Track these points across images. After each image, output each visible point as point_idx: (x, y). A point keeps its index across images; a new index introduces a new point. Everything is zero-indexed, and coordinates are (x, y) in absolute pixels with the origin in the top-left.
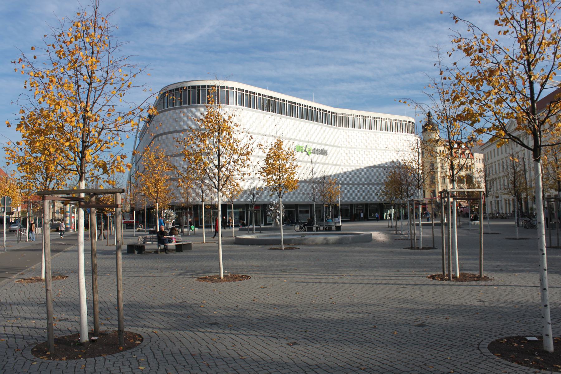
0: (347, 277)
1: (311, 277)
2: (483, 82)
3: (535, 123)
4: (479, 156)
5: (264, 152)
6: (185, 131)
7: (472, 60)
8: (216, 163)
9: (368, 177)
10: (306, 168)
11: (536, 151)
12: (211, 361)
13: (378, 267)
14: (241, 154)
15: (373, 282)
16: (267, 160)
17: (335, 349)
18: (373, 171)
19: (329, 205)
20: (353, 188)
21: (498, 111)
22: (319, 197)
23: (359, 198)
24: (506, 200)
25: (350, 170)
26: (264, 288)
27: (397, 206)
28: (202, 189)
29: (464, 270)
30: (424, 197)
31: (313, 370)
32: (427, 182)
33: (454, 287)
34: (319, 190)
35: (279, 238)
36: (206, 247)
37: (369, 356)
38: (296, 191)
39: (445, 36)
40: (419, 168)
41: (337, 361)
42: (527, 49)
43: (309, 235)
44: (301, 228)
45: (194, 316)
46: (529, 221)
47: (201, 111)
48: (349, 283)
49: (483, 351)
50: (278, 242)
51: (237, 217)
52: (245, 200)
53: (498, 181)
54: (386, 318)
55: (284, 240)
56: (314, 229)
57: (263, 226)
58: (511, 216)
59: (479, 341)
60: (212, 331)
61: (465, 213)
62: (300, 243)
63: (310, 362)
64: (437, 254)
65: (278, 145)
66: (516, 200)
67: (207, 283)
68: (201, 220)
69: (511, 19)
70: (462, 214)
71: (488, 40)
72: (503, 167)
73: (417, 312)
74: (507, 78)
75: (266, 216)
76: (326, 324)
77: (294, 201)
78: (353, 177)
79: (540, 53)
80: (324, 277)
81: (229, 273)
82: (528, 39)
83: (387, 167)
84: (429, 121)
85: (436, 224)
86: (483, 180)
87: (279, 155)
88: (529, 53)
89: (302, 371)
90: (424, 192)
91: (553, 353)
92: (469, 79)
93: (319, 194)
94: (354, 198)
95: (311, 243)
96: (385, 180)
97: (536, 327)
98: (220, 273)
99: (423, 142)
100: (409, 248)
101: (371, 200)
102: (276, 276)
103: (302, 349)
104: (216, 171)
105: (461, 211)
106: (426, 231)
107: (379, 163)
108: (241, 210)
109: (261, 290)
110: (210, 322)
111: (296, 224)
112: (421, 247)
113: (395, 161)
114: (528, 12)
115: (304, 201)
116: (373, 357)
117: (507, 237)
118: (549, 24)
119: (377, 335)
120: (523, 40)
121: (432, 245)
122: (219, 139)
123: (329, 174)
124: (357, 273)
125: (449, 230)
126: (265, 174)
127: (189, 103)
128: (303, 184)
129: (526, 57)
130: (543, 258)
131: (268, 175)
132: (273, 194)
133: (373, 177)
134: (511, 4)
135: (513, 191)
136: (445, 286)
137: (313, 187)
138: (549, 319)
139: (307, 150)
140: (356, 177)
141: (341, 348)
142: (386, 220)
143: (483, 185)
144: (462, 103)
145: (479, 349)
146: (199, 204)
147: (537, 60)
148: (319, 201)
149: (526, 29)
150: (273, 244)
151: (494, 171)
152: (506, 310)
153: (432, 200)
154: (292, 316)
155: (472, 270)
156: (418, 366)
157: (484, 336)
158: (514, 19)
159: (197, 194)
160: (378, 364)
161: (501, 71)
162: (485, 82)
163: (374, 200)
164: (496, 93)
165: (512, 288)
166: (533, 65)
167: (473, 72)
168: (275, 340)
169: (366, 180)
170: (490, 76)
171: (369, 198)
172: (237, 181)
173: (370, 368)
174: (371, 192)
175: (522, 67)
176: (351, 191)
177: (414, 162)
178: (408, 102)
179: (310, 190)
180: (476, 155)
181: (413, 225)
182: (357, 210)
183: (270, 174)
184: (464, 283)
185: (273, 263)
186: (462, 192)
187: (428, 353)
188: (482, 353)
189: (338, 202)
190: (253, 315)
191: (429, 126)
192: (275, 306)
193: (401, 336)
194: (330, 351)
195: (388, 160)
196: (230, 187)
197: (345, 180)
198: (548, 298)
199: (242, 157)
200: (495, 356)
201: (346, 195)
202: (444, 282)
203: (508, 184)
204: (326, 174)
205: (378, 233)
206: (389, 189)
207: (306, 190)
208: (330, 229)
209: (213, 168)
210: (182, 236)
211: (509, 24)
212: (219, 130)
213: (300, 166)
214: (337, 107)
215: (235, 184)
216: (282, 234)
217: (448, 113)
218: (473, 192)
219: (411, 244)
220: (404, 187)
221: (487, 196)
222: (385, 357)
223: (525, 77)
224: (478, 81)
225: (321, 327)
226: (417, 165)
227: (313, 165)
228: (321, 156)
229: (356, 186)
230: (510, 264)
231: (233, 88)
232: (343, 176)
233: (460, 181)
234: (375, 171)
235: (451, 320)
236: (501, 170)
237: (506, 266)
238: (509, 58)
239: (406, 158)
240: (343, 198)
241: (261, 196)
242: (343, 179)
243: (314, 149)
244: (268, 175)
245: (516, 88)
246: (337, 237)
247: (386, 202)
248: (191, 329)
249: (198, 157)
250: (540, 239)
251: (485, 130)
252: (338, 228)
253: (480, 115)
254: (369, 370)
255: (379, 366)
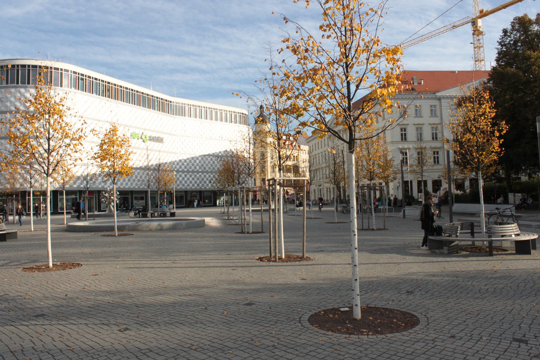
0: (179, 262)
1: (144, 262)
2: (308, 80)
3: (351, 119)
4: (305, 148)
5: (99, 138)
6: (11, 112)
7: (299, 58)
8: (46, 147)
9: (202, 165)
10: (141, 155)
11: (351, 143)
12: (34, 356)
13: (210, 251)
14: (72, 138)
15: (205, 265)
16: (101, 146)
17: (167, 332)
18: (207, 159)
19: (164, 192)
20: (188, 176)
21: (320, 107)
22: (154, 184)
23: (193, 185)
24: (327, 188)
25: (185, 158)
26: (95, 275)
27: (229, 193)
28: (30, 174)
29: (289, 252)
30: (255, 185)
31: (144, 354)
32: (258, 170)
33: (279, 267)
34: (154, 177)
35: (113, 224)
36: (34, 235)
37: (199, 336)
38: (132, 177)
39: (275, 35)
40: (249, 158)
41: (169, 344)
42: (345, 53)
43: (143, 221)
44: (135, 214)
45: (17, 309)
46: (346, 207)
47: (30, 92)
48: (182, 267)
49: (303, 324)
50: (112, 229)
51: (70, 204)
52: (78, 186)
53: (321, 171)
54: (216, 299)
55: (118, 226)
56: (149, 215)
57: (96, 213)
58: (332, 203)
59: (301, 315)
60: (37, 323)
61: (291, 199)
62: (134, 229)
63: (142, 346)
64: (265, 237)
65: (113, 131)
66: (336, 188)
67: (34, 273)
68: (29, 207)
69: (333, 25)
70: (288, 201)
71: (313, 42)
72: (325, 158)
73: (245, 292)
74: (328, 77)
75: (100, 203)
76: (159, 307)
77: (129, 187)
78: (188, 164)
79: (356, 58)
80: (157, 262)
81: (58, 261)
82: (347, 45)
83: (220, 156)
84: (261, 113)
85: (265, 210)
86: (308, 170)
87: (113, 141)
88: (347, 57)
89: (133, 356)
90: (255, 180)
91: (360, 320)
92: (296, 76)
93: (154, 181)
94: (188, 185)
95: (145, 229)
96: (218, 168)
97: (348, 299)
98: (48, 261)
99: (255, 133)
100: (240, 233)
101: (205, 188)
102: (109, 263)
103: (134, 334)
104: (46, 155)
105: (288, 198)
106: (256, 216)
107: (214, 152)
108: (74, 196)
109: (93, 277)
110: (36, 314)
111: (131, 210)
112: (251, 232)
113: (228, 150)
114: (348, 21)
115: (139, 187)
116: (204, 337)
117: (327, 221)
118: (364, 33)
119: (207, 316)
120: (344, 45)
121: (260, 230)
122: (49, 123)
123: (165, 162)
124: (189, 257)
125: (275, 215)
126: (99, 160)
127: (18, 83)
128: (139, 171)
129: (344, 60)
130: (354, 238)
131: (102, 161)
132: (108, 180)
133: (207, 165)
134: (334, 12)
135: (333, 181)
136: (272, 267)
137: (148, 174)
138: (358, 291)
139: (143, 137)
140: (190, 165)
141: (173, 330)
142: (219, 206)
143: (308, 174)
144: (289, 98)
145: (300, 322)
146: (28, 190)
147: (353, 64)
148: (155, 188)
149: (345, 36)
150: (106, 231)
151: (318, 162)
152: (324, 286)
153: (261, 187)
154: (124, 302)
155: (296, 252)
156: (246, 342)
157: (305, 311)
158: (336, 25)
159: (25, 180)
160: (209, 343)
161: (323, 70)
162: (310, 80)
163: (208, 188)
164: (318, 90)
165: (330, 266)
166: (350, 67)
167: (299, 69)
168: (106, 327)
169: (200, 168)
170: (314, 74)
171: (203, 185)
172: (69, 167)
173: (201, 347)
174: (205, 180)
175: (341, 69)
176: (186, 179)
177: (245, 151)
178: (240, 95)
179: (146, 177)
180: (302, 147)
181: (244, 211)
182: (191, 196)
183: (104, 160)
184: (289, 263)
185: (105, 249)
186: (289, 180)
187: (255, 329)
188: (302, 326)
189: (173, 188)
190: (83, 304)
191: (261, 119)
192: (106, 293)
193: (230, 316)
194: (162, 334)
195: (222, 149)
196: (61, 173)
197: (180, 167)
198: (358, 273)
199: (74, 142)
200: (314, 328)
201: (181, 182)
202: (271, 263)
203: (329, 173)
204: (161, 162)
205: (211, 218)
206: (222, 176)
207: (141, 177)
208: (164, 215)
209: (43, 152)
210: (5, 224)
211: (332, 30)
212: (49, 113)
213: (136, 153)
214: (174, 96)
215: (66, 169)
216: (116, 221)
217: (277, 108)
218: (298, 180)
219: (242, 229)
220: (236, 175)
221: (311, 185)
222: (216, 336)
223: (344, 77)
224: (303, 78)
225: (153, 312)
226: (248, 155)
227: (149, 152)
228: (157, 144)
229: (191, 174)
230: (328, 245)
231: (68, 71)
232: (178, 164)
233: (288, 170)
234: (209, 159)
235: (276, 297)
236: (324, 161)
237: (325, 247)
238: (331, 60)
239: (238, 148)
240: (178, 185)
241: (94, 182)
242: (178, 166)
243: (150, 137)
244: (102, 161)
245: (335, 87)
246: (171, 223)
247: (219, 189)
248: (13, 324)
249: (25, 140)
250: (351, 222)
251: (309, 124)
252: (173, 215)
253: (305, 109)
254: (200, 349)
255: (209, 345)
